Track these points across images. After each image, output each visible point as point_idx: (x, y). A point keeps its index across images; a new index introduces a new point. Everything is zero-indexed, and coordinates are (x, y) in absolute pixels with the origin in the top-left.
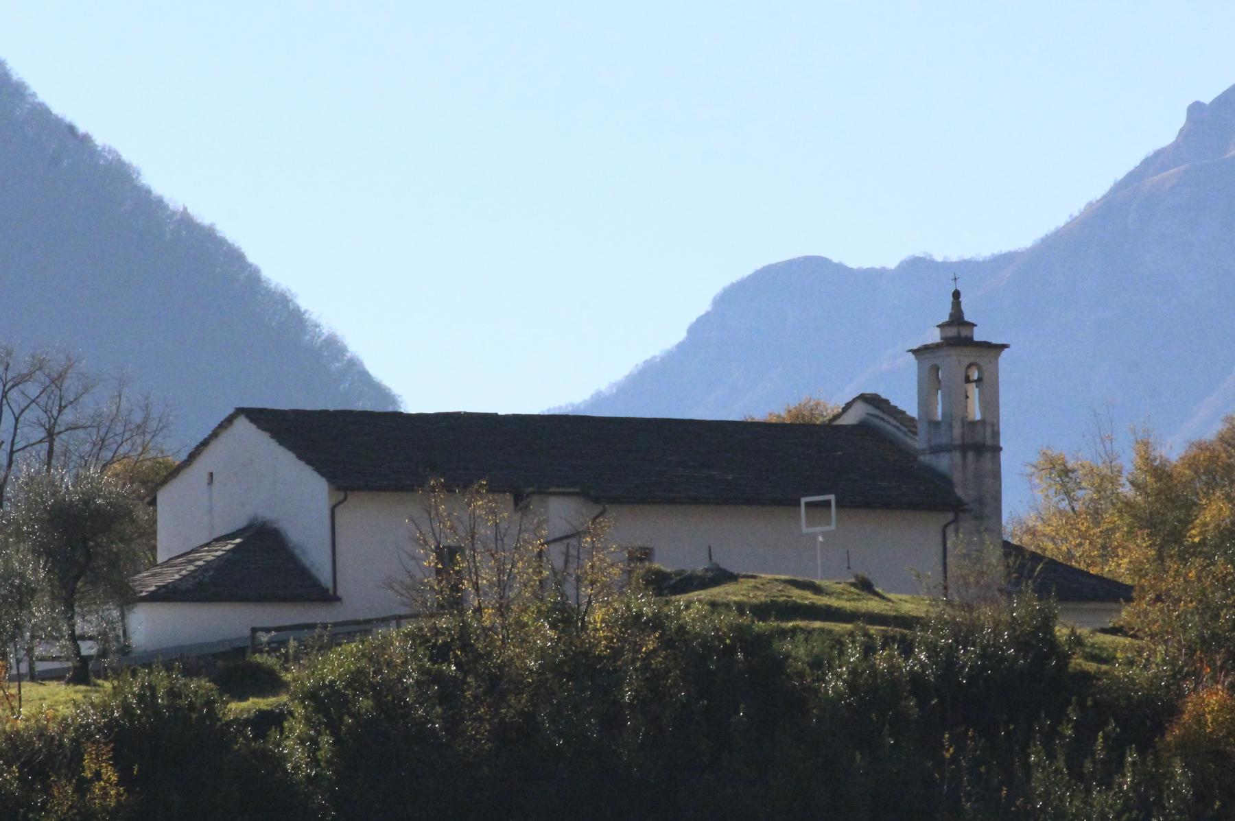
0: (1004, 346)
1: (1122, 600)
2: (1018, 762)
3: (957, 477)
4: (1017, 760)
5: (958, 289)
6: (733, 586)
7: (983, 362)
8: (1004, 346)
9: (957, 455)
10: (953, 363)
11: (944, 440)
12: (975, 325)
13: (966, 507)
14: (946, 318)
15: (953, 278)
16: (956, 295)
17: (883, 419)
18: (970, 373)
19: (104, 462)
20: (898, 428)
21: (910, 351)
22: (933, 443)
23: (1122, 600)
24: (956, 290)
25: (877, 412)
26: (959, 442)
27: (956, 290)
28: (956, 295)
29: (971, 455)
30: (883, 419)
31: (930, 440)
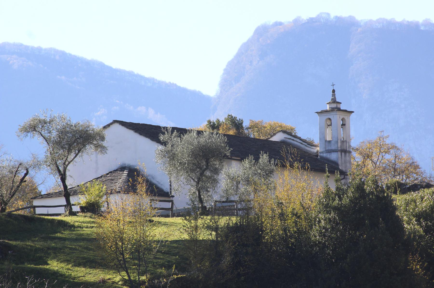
0: (352, 112)
1: (392, 198)
2: (242, 269)
3: (340, 163)
4: (241, 268)
5: (334, 89)
6: (63, 220)
7: (346, 118)
8: (352, 112)
9: (339, 153)
10: (337, 118)
11: (333, 147)
12: (341, 103)
13: (346, 174)
14: (330, 101)
15: (332, 84)
16: (334, 91)
17: (293, 140)
18: (330, 122)
19: (198, 199)
20: (301, 143)
21: (316, 112)
22: (327, 149)
23: (392, 198)
24: (333, 89)
25: (289, 137)
26: (340, 149)
27: (333, 89)
28: (334, 91)
29: (343, 154)
30: (293, 140)
31: (325, 148)
